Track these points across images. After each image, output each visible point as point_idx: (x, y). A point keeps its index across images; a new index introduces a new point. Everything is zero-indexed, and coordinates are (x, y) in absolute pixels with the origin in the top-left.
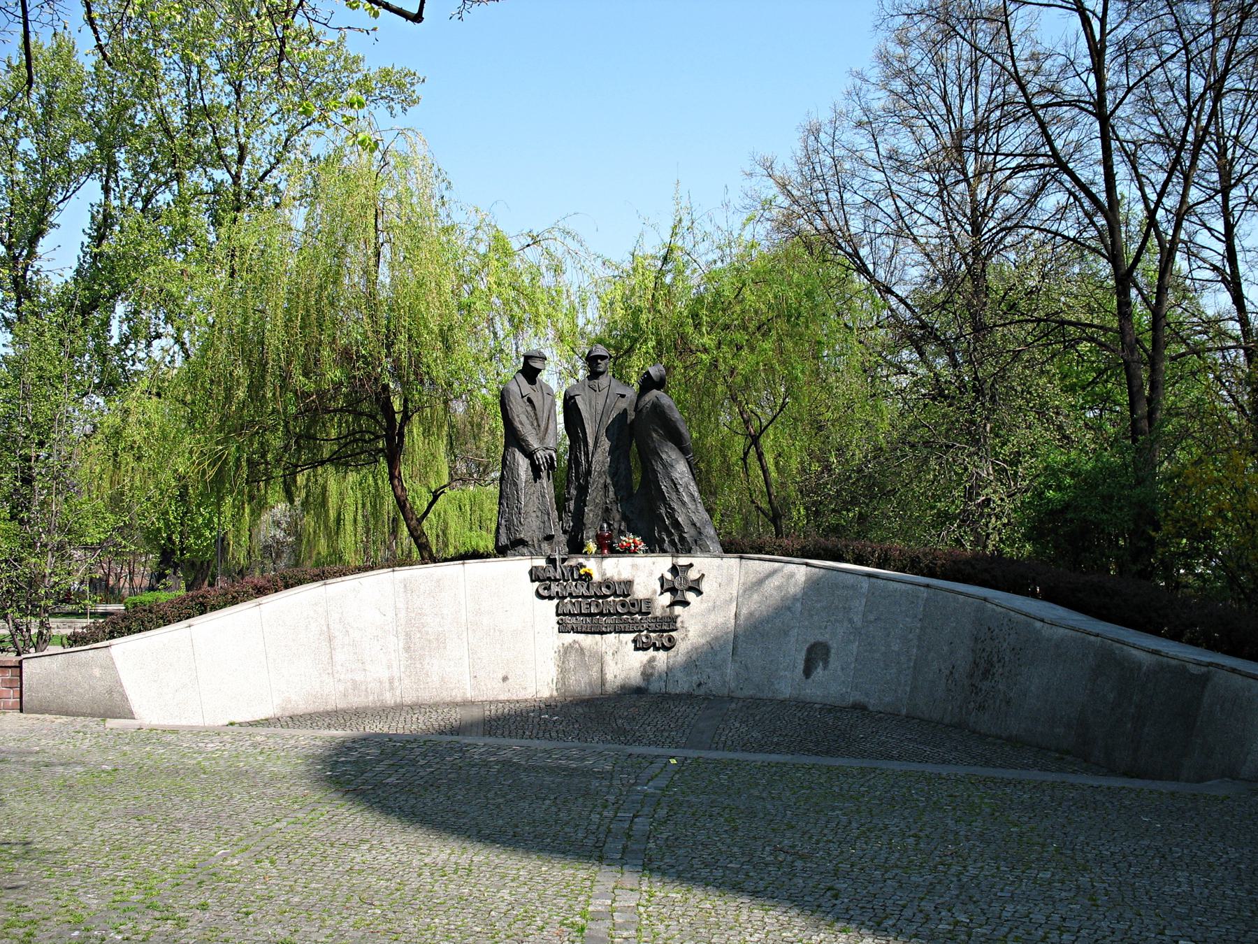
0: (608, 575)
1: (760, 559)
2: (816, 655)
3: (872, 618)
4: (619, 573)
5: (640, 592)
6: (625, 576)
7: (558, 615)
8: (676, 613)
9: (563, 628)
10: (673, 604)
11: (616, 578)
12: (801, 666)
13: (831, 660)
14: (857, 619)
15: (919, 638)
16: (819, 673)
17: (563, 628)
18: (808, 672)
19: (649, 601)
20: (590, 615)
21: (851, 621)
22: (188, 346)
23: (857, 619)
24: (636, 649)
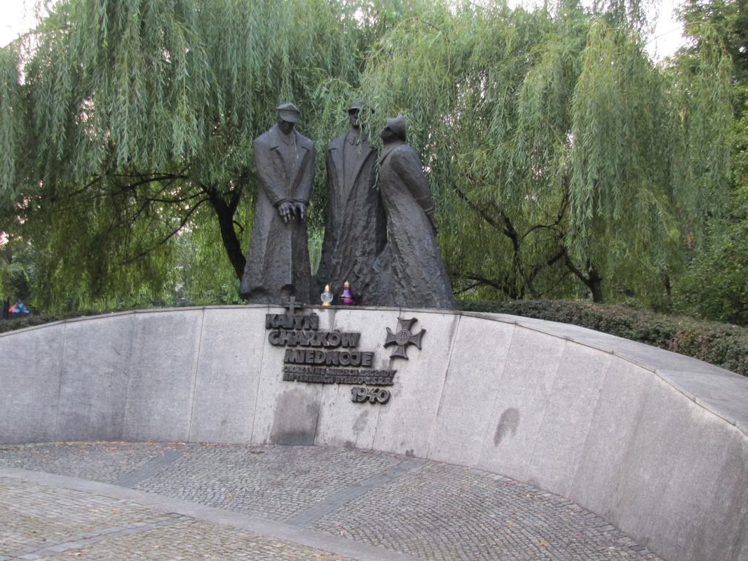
0: (338, 327)
1: (29, 330)
2: (508, 420)
3: (560, 385)
4: (350, 325)
5: (365, 345)
6: (354, 329)
7: (285, 363)
8: (394, 368)
9: (289, 377)
10: (393, 358)
11: (345, 330)
12: (493, 432)
13: (519, 428)
14: (548, 385)
15: (595, 412)
16: (506, 439)
17: (289, 377)
18: (498, 438)
19: (372, 355)
20: (313, 364)
21: (543, 387)
22: (675, 193)
23: (548, 385)
24: (355, 401)
